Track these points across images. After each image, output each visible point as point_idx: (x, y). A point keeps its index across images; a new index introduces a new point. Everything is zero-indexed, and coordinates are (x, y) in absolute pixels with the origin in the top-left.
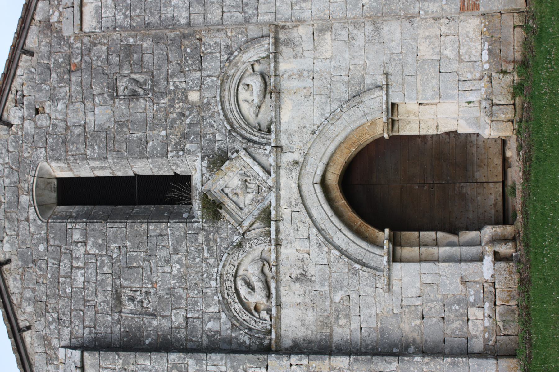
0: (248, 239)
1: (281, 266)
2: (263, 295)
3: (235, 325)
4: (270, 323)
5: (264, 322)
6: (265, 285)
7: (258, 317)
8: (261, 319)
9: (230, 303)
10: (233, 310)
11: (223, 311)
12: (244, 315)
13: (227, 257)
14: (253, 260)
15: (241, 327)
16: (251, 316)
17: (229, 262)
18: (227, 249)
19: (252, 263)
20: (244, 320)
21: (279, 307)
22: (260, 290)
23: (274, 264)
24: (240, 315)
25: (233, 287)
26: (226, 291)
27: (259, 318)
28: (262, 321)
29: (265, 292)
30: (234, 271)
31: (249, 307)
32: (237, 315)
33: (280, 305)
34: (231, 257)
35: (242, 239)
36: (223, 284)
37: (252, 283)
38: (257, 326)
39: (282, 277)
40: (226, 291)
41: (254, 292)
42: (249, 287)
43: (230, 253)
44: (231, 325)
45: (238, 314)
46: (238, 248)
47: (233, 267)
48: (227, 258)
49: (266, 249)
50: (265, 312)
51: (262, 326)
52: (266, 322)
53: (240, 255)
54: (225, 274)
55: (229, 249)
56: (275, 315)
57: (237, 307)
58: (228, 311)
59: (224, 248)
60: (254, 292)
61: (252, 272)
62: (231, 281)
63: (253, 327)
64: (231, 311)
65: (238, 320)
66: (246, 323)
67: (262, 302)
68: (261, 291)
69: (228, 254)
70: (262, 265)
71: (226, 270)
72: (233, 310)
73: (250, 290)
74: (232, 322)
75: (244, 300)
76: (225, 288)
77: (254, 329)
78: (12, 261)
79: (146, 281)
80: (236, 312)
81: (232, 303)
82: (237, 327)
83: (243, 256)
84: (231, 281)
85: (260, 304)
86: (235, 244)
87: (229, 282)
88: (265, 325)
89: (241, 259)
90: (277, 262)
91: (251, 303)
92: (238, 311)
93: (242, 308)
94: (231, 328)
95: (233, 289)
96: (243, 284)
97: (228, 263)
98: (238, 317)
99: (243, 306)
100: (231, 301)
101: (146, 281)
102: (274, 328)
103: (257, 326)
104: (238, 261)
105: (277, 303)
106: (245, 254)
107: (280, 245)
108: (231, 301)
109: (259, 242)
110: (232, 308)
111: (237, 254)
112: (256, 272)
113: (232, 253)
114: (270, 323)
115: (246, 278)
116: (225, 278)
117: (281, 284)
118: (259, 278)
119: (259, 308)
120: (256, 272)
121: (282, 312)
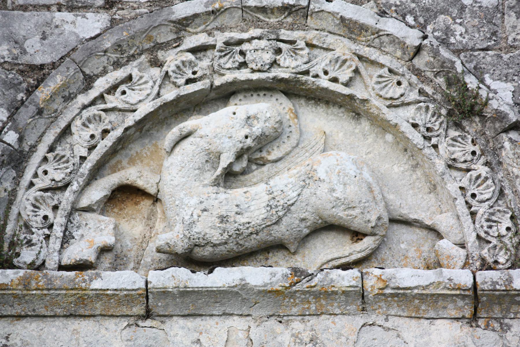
0: (496, 151)
1: (360, 320)
2: (198, 228)
3: (40, 81)
4: (52, 263)
5: (58, 231)
6: (252, 243)
7: (84, 202)
8: (69, 216)
9: (157, 63)
10: (120, 74)
11: (113, 22)
12: (95, 129)
13: (400, 43)
14: (380, 179)
15: (32, 109)
16: (88, 166)
17: (374, 54)
18: (444, 42)
19: (367, 175)
20: (67, 131)
21: (139, 310)
22: (229, 209)
23: (370, 283)
24: (93, 110)
25: (244, 75)
26: (220, 39)
27: (75, 209)
28: (59, 220)
29: (215, 237)
30: (324, 83)
31: (132, 162)
32: (93, 94)
33: (148, 315)
34: (395, 65)
35: (500, 116)
36: (257, 24)
37: (257, 173)
38: (33, 193)
39: (297, 325)
40: (220, 39)
41: (216, 183)
42: (239, 156)
43: (419, 62)
44: (38, 60)
45: (101, 97)
46: (448, 99)
47: (345, 75)
48: (394, 40)
49: (445, 245)
50: (109, 239)
51: (36, 222)
52: (55, 244)
53: (410, 112)
54: (311, 35)
55: (445, 53)
56: (97, 284)
57: (132, 97)
58: (118, 47)
59: (448, 31)
60: (216, 183)
61: (321, 173)
62: (274, 63)
63: (28, 176)
64: (117, 65)
65: (69, 98)
66: (50, 138)
67: (159, 226)
68: (223, 219)
69: (418, 50)
70: (357, 224)
71: (331, 39)
72: (120, 74)
73: (224, 163)
74: (54, 66)
75: (174, 132)
76: (237, 35)
77: (17, 181)
78: (402, 86)
79: (403, 6)
80: (112, 89)
81: (156, 73)
82: (29, 92)
83: (406, 128)
84: (274, 63)
85: (151, 217)
86: (471, 82)
87: (268, 57)
88: (37, 237)
89: (391, 115)
90: (381, 295)
91: (159, 170)
92: (113, 101)
93: (130, 120)
94: (25, 59)
95: (229, 77)
96: (257, 129)
97: (365, 51)
98: (83, 99)
99: (140, 124)
100: (170, 66)
101: (403, 6)
102: (25, 283)
103: (33, 193)
104: (376, 102)
105: (164, 293)
106: (416, 138)
107: (475, 317)
108: (170, 66)
109: (482, 210)
110: (132, 69)
111: (413, 96)
112: (324, 188)
113: (418, 72)
114: (52, 263)
115: (285, 147)
116: (285, 34)
117: (259, 321)
118: (288, 209)
119: (129, 209)
120: (323, 190)
121: (111, 324)
